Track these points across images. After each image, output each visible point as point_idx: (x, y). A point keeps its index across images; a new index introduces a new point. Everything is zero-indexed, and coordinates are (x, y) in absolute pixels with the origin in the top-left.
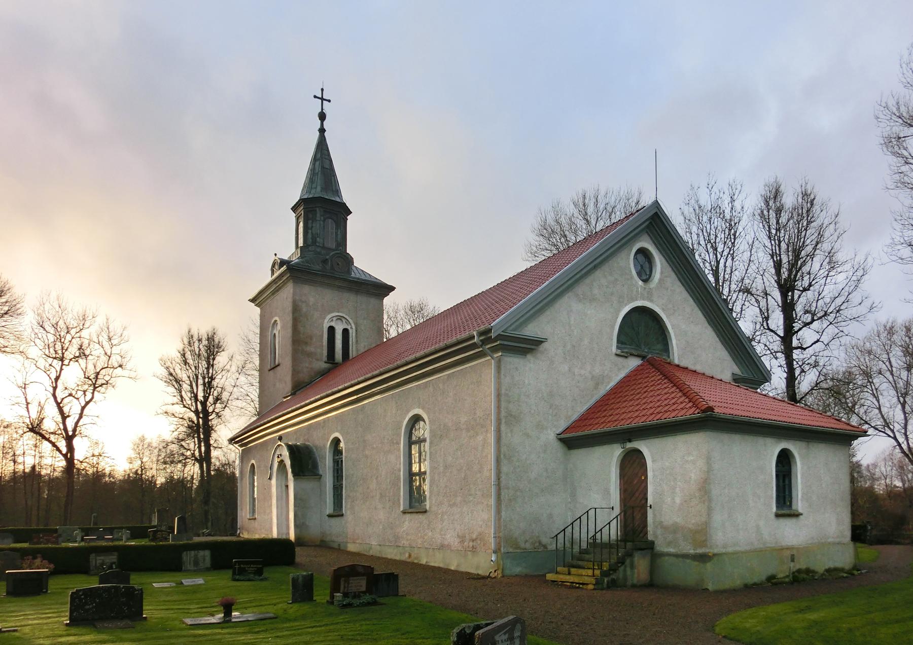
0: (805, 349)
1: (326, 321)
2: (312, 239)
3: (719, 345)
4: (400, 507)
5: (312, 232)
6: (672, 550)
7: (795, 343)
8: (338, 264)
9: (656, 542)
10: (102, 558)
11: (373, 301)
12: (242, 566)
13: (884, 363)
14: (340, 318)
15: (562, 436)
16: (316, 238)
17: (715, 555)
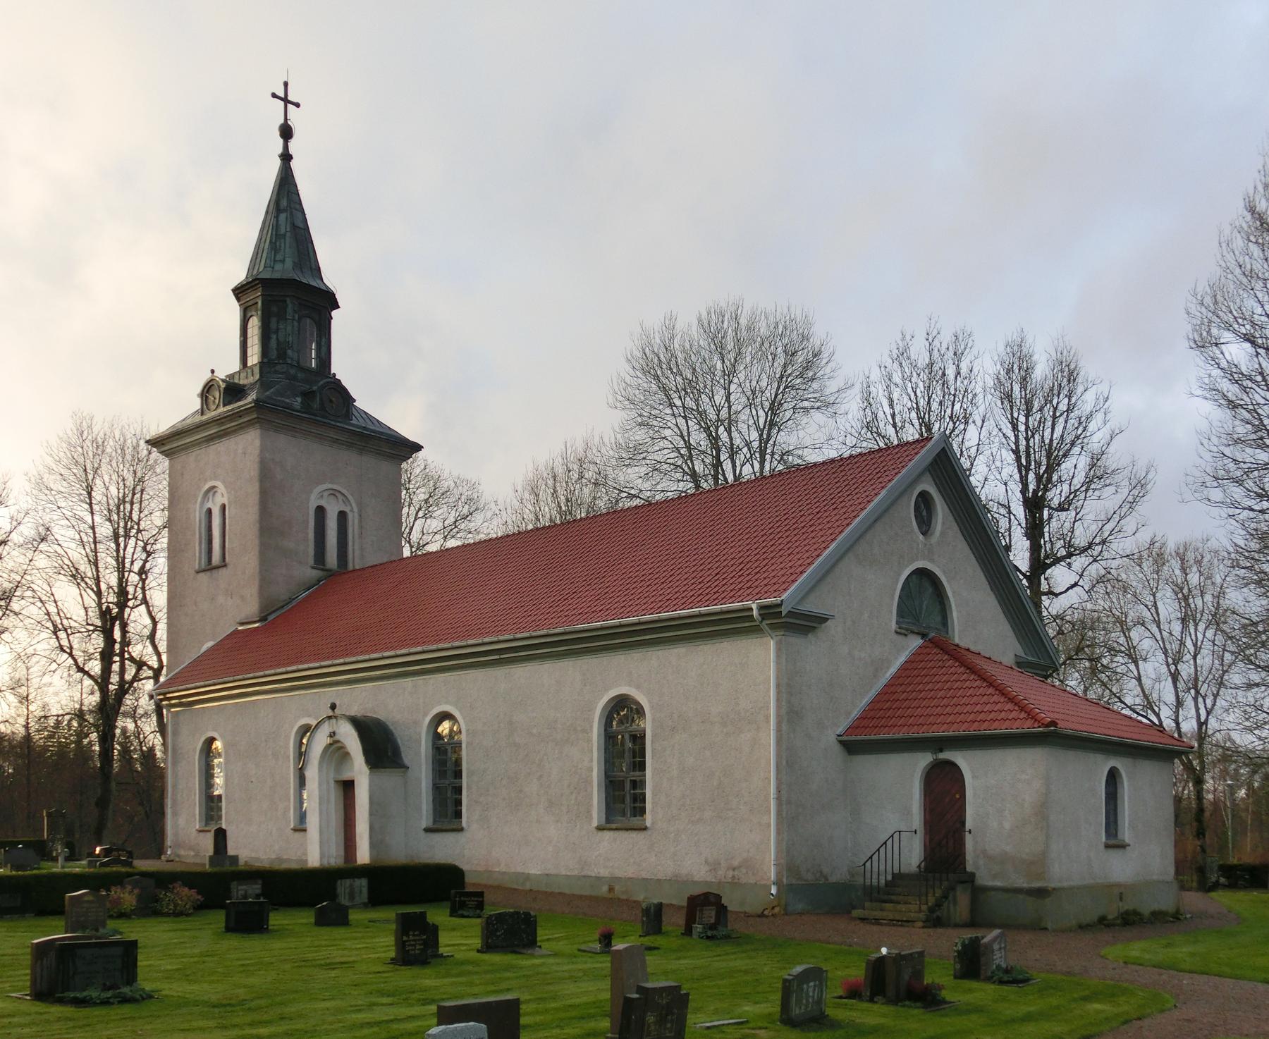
0: (1057, 595)
1: (313, 497)
3: (1002, 617)
4: (591, 818)
5: (277, 339)
6: (998, 883)
7: (1044, 587)
8: (331, 401)
9: (977, 875)
10: (244, 887)
11: (385, 466)
13: (1149, 610)
14: (334, 493)
15: (845, 738)
17: (1054, 889)
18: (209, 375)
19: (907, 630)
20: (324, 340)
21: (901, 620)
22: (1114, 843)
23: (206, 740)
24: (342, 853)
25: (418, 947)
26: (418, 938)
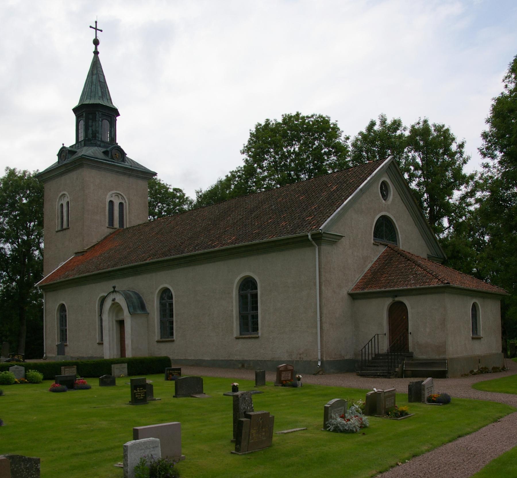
1: (108, 197)
2: (92, 134)
5: (92, 130)
12: (171, 372)
14: (117, 195)
16: (96, 134)
18: (62, 146)
19: (378, 243)
20: (113, 129)
21: (375, 238)
22: (476, 337)
23: (60, 305)
24: (120, 353)
25: (142, 395)
26: (142, 391)
